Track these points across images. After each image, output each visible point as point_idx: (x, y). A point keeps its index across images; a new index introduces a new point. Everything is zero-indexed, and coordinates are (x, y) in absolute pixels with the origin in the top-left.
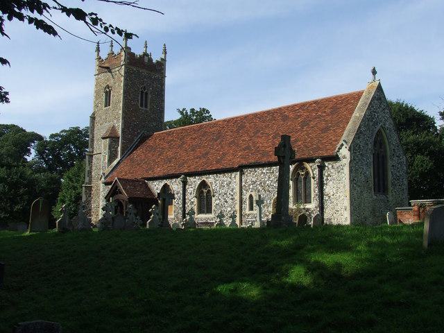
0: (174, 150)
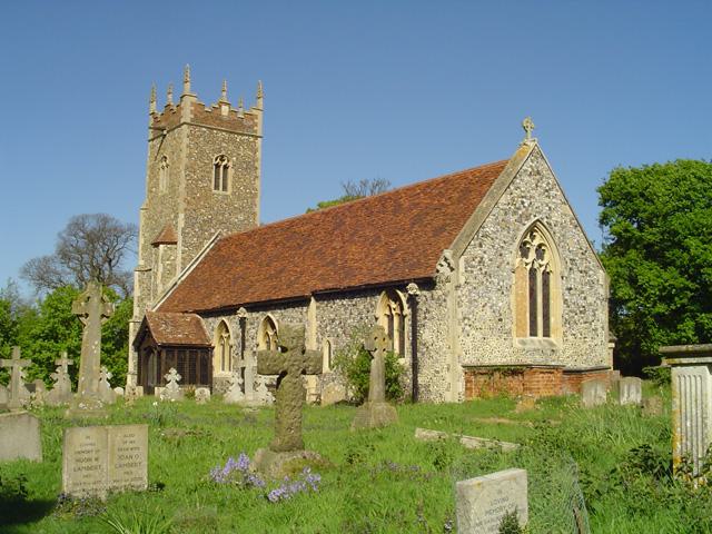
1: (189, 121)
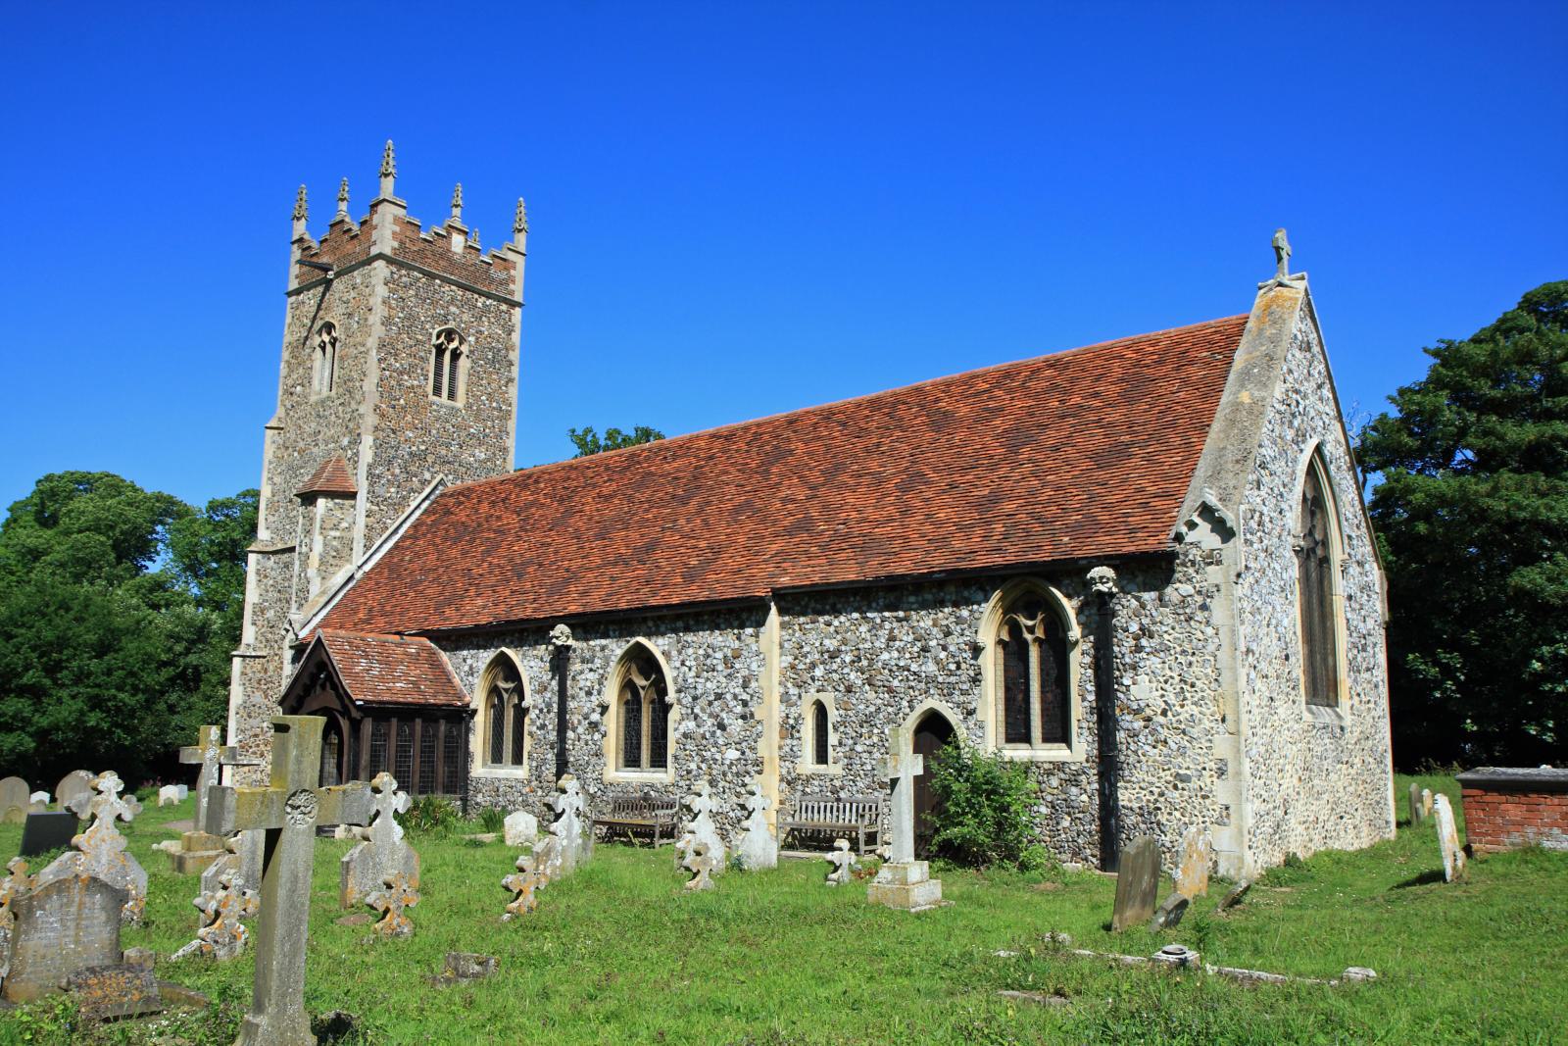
0: (536, 537)
1: (388, 251)
